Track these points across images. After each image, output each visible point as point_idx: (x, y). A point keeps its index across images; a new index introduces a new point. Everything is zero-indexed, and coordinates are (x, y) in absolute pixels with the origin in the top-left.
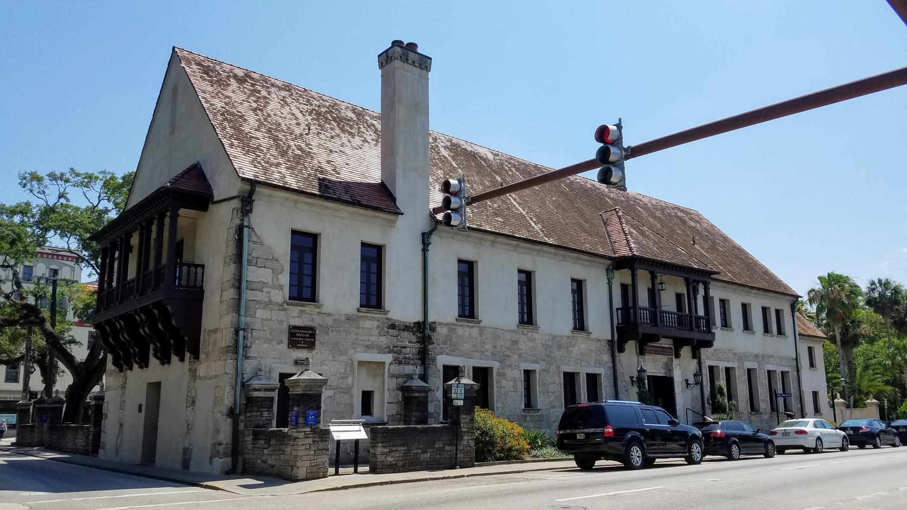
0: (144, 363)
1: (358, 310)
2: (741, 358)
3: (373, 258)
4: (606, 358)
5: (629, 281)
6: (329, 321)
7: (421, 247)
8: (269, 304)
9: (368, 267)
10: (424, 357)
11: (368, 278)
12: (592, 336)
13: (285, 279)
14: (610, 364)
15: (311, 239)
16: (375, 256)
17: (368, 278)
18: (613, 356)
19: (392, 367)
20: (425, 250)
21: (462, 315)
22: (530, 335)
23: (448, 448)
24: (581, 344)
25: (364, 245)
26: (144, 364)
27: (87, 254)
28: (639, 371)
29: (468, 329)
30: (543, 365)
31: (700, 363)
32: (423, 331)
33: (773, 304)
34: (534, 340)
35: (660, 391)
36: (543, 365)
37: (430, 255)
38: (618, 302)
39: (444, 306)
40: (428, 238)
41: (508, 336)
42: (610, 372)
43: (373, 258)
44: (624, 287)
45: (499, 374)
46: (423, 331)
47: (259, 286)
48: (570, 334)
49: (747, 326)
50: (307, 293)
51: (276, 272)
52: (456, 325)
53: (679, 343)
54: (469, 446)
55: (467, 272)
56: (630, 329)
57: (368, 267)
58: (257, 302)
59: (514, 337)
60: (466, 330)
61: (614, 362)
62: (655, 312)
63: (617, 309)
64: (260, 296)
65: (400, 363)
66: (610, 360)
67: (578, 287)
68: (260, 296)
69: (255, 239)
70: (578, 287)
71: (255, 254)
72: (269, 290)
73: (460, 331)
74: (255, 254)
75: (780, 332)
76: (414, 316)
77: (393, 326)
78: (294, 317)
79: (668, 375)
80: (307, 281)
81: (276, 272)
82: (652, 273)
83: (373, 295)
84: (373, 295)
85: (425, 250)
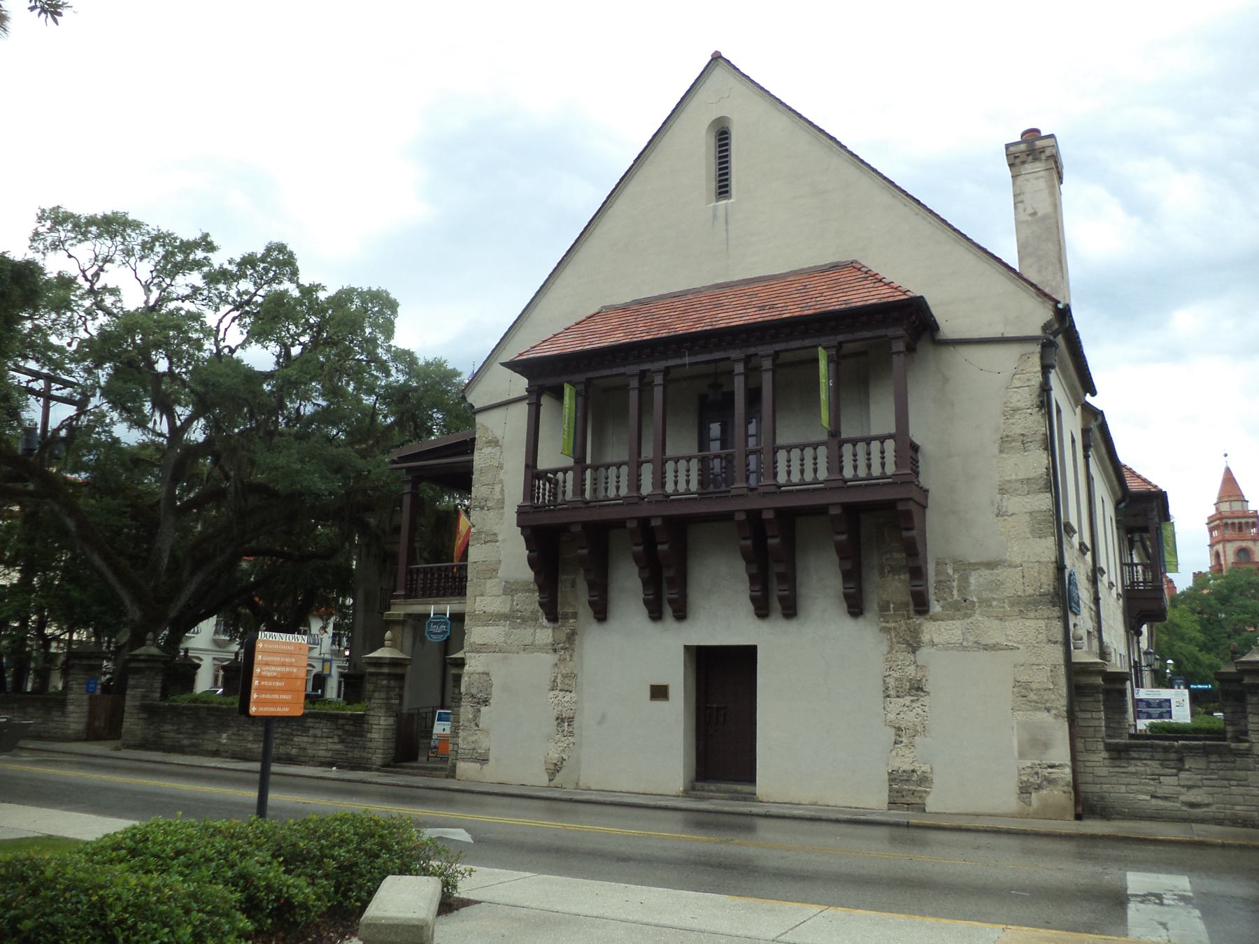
26: (667, 599)
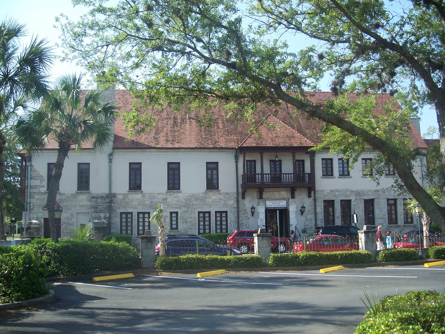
0: (228, 259)
6: (63, 197)
8: (40, 193)
10: (110, 209)
12: (220, 192)
18: (238, 201)
19: (93, 214)
20: (110, 161)
22: (175, 195)
27: (19, 186)
30: (184, 209)
32: (110, 197)
35: (278, 222)
39: (121, 185)
41: (160, 196)
46: (110, 197)
47: (35, 187)
51: (42, 181)
56: (250, 184)
58: (35, 193)
59: (164, 196)
61: (238, 204)
64: (36, 190)
65: (97, 212)
68: (36, 190)
69: (34, 170)
71: (34, 175)
73: (130, 196)
74: (34, 175)
76: (105, 190)
77: (93, 197)
81: (42, 181)
85: (110, 161)
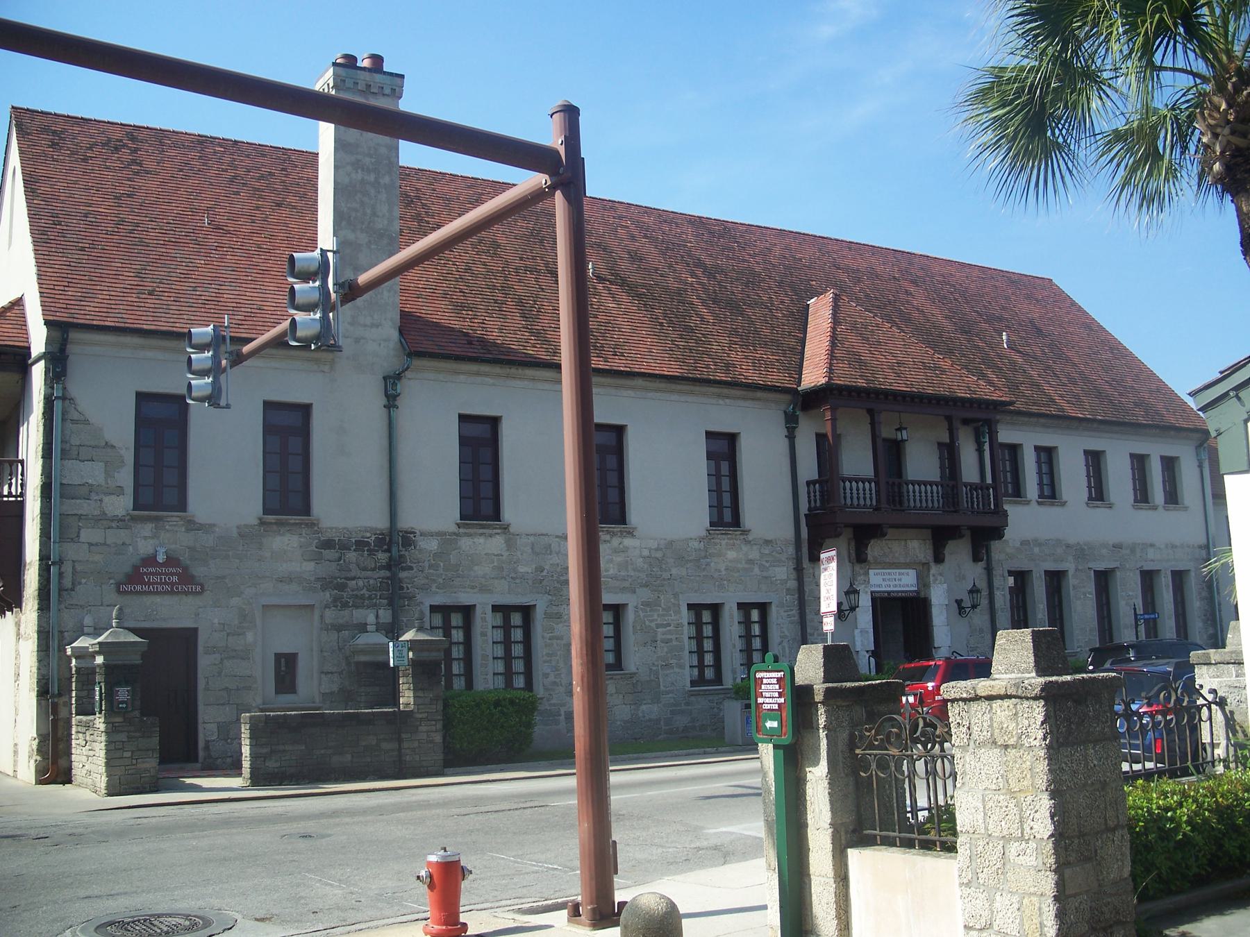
1: (459, 526)
2: (1081, 552)
3: (288, 429)
4: (783, 572)
5: (828, 429)
7: (384, 401)
8: (102, 520)
9: (718, 469)
11: (719, 483)
13: (125, 477)
14: (793, 584)
15: (487, 427)
16: (614, 443)
17: (719, 483)
21: (717, 522)
23: (385, 746)
24: (730, 552)
25: (710, 435)
28: (971, 592)
29: (482, 540)
30: (645, 594)
31: (989, 570)
32: (393, 544)
33: (1155, 450)
34: (625, 550)
36: (645, 594)
37: (798, 441)
38: (808, 468)
39: (433, 502)
40: (394, 384)
42: (792, 599)
43: (288, 429)
44: (821, 438)
45: (548, 616)
46: (393, 544)
48: (453, 528)
49: (1098, 493)
50: (487, 507)
51: (111, 467)
52: (457, 535)
53: (940, 537)
54: (432, 742)
55: (480, 442)
57: (718, 469)
60: (484, 545)
62: (954, 487)
63: (808, 483)
64: (85, 507)
65: (345, 605)
66: (793, 575)
67: (723, 450)
68: (85, 507)
69: (75, 416)
70: (723, 450)
72: (101, 496)
73: (465, 543)
74: (75, 441)
75: (1172, 497)
76: (373, 518)
77: (328, 544)
78: (145, 538)
79: (922, 595)
80: (486, 490)
81: (111, 467)
82: (870, 412)
83: (288, 489)
84: (288, 489)
